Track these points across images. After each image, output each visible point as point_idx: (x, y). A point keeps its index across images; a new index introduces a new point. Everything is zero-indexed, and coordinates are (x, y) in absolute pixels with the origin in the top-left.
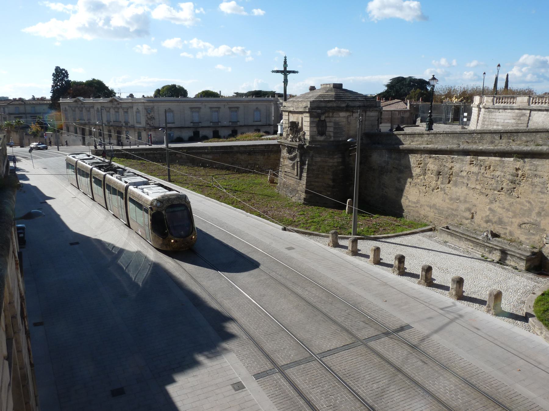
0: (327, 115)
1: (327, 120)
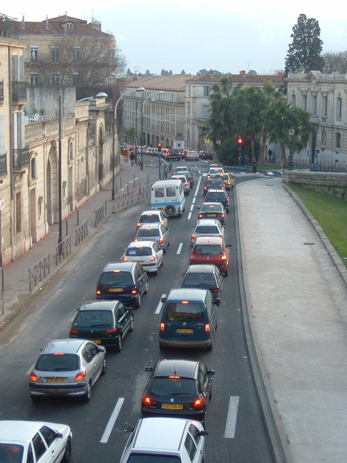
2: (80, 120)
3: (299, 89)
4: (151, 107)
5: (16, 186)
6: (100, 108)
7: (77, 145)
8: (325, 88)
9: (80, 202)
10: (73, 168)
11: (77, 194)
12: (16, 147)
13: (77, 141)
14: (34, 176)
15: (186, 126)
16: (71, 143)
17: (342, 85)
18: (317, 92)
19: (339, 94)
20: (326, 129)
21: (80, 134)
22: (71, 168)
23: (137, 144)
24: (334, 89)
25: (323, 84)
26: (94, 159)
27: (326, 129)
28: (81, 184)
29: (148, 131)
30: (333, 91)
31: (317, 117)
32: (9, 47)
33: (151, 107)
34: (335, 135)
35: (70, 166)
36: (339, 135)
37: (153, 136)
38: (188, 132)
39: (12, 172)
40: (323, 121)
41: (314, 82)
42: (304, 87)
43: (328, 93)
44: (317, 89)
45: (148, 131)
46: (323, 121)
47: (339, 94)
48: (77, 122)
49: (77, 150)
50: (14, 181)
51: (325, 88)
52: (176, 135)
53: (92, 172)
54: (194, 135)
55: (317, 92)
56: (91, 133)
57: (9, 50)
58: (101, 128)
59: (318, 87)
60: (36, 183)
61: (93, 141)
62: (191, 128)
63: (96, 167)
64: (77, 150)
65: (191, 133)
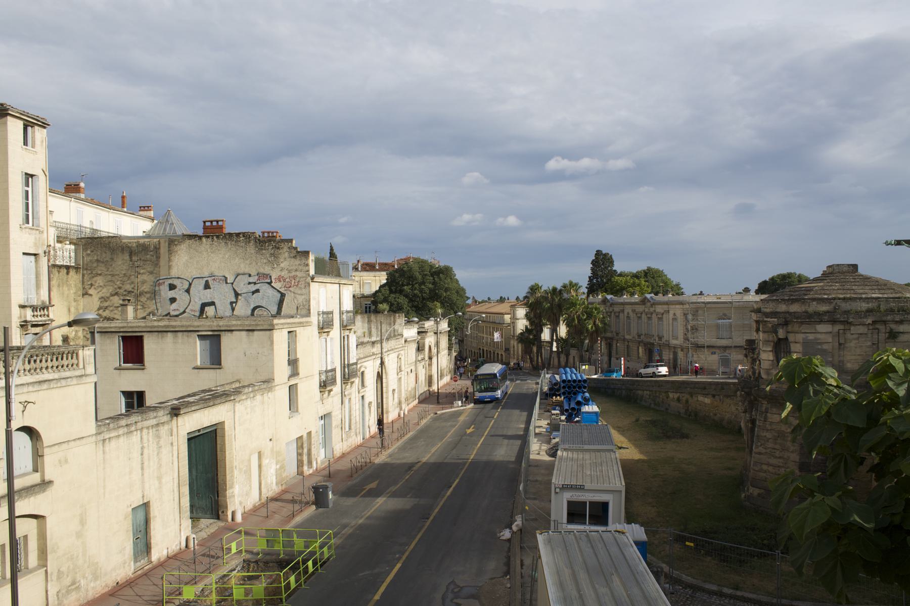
0: (790, 328)
1: (791, 337)
2: (408, 340)
3: (634, 311)
4: (485, 327)
5: (346, 393)
6: (428, 329)
7: (406, 359)
8: (659, 309)
9: (410, 406)
10: (403, 378)
11: (407, 399)
12: (346, 363)
13: (406, 356)
14: (363, 385)
15: (512, 342)
16: (400, 358)
17: (630, 306)
18: (611, 312)
19: (628, 313)
20: (630, 344)
21: (409, 351)
22: (401, 378)
23: (626, 354)
24: (669, 311)
25: (615, 306)
26: (424, 371)
27: (379, 345)
28: (410, 392)
29: (483, 347)
30: (623, 311)
31: (612, 332)
32: (339, 284)
33: (485, 327)
34: (626, 347)
35: (400, 376)
36: (628, 347)
37: (487, 350)
38: (514, 347)
39: (343, 382)
40: (617, 336)
41: (608, 304)
42: (640, 308)
43: (619, 312)
44: (611, 310)
45: (483, 347)
46: (617, 336)
47: (628, 313)
48: (406, 341)
49: (406, 363)
50: (345, 389)
51: (617, 309)
52: (504, 349)
53: (422, 381)
54: (518, 349)
55: (611, 312)
56: (420, 349)
57: (340, 286)
58: (430, 346)
59: (611, 308)
60: (365, 391)
61: (423, 356)
62: (515, 344)
63: (426, 377)
64: (406, 363)
65: (516, 348)
